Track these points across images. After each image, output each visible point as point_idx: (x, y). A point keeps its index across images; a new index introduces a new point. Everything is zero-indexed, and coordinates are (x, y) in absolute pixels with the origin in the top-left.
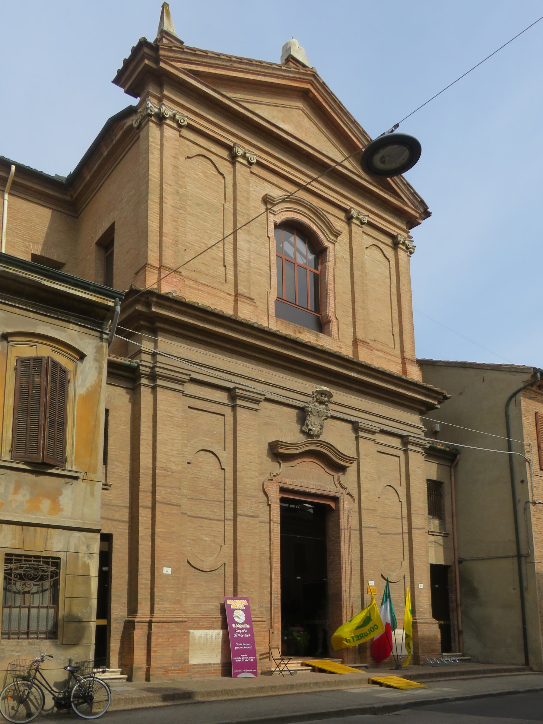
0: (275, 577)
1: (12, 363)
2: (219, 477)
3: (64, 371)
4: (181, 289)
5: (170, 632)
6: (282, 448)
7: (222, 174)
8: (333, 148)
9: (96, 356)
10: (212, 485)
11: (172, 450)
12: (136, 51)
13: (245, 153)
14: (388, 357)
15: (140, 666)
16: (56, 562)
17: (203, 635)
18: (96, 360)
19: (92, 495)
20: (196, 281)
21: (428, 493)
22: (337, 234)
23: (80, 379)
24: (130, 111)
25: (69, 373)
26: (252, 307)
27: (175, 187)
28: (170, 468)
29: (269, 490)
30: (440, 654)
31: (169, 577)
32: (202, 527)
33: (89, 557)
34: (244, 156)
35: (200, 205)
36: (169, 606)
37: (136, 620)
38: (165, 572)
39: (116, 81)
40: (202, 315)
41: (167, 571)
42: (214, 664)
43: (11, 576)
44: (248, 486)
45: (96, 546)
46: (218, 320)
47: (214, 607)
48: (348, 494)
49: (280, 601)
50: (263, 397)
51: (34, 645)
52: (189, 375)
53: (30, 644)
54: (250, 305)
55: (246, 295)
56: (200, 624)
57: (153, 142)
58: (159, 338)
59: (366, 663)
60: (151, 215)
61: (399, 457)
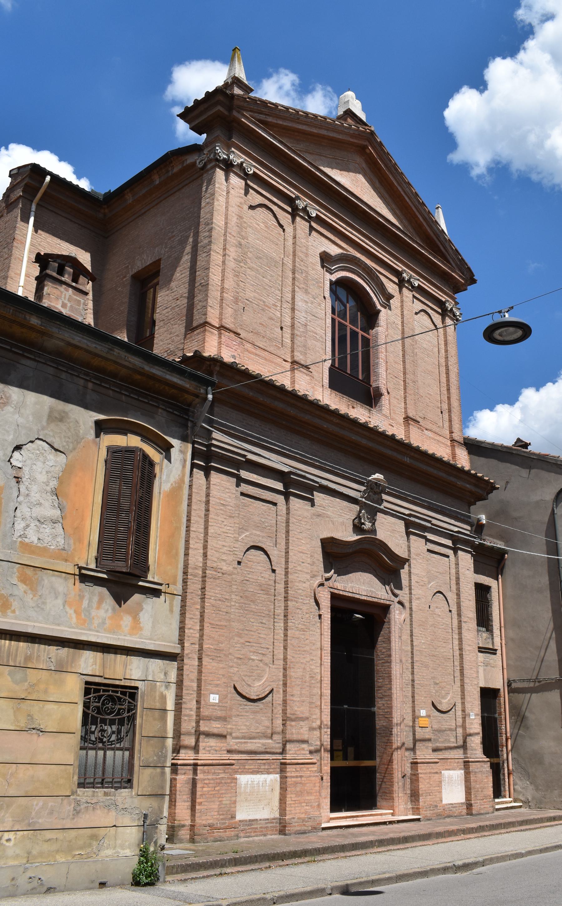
0: (325, 707)
1: (103, 454)
3: (151, 464)
4: (240, 354)
5: (217, 779)
7: (281, 226)
9: (181, 447)
10: (262, 590)
14: (438, 438)
15: (182, 823)
16: (131, 692)
17: (250, 782)
18: (181, 451)
19: (171, 611)
21: (476, 600)
23: (165, 474)
24: (194, 149)
26: (308, 378)
27: (239, 239)
28: (221, 569)
29: (320, 596)
30: (492, 801)
31: (216, 707)
33: (167, 687)
34: (305, 210)
35: (260, 258)
36: (215, 745)
38: (211, 701)
41: (214, 698)
42: (260, 820)
43: (89, 709)
51: (110, 796)
52: (244, 456)
53: (106, 794)
54: (307, 375)
55: (302, 362)
56: (246, 767)
57: (219, 188)
59: (419, 814)
60: (213, 267)
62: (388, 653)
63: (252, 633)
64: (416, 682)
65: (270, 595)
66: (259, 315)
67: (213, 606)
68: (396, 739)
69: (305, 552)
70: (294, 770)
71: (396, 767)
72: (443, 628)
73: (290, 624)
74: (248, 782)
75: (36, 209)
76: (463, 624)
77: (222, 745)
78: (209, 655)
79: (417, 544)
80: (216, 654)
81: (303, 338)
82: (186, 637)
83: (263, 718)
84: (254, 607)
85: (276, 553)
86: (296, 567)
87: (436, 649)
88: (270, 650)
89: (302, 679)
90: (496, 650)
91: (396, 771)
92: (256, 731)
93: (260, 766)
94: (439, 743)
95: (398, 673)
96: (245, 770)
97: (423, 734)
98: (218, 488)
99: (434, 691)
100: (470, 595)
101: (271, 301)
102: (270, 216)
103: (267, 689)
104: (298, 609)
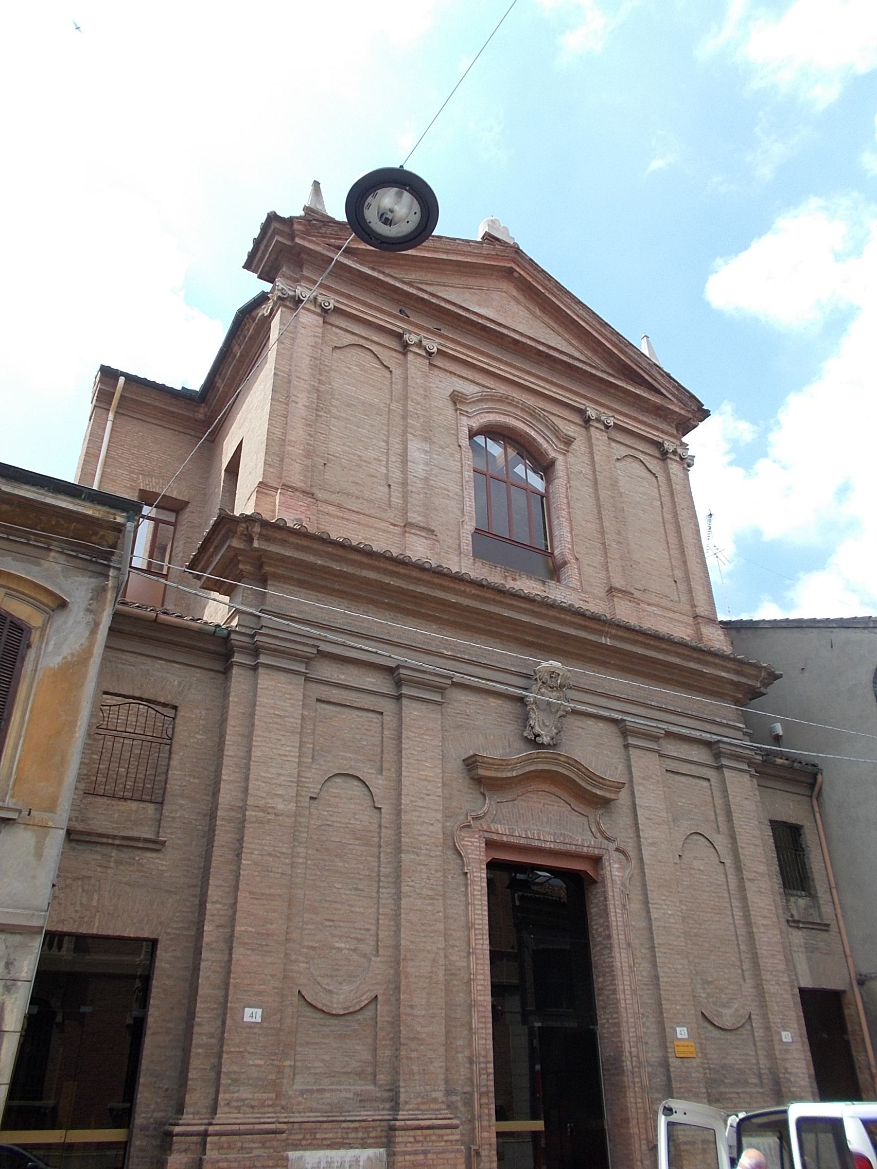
2: (370, 823)
6: (486, 769)
8: (554, 335)
10: (357, 839)
11: (279, 774)
12: (265, 228)
13: (421, 341)
14: (671, 615)
19: (39, 854)
20: (339, 506)
22: (568, 441)
23: (52, 642)
24: (262, 298)
25: (33, 631)
28: (274, 808)
31: (256, 1030)
32: (332, 921)
34: (419, 345)
36: (250, 1096)
37: (177, 1129)
39: (248, 266)
40: (631, 636)
41: (252, 1015)
44: (423, 838)
45: (26, 962)
46: (365, 560)
47: (350, 1095)
48: (617, 850)
49: (492, 1077)
50: (449, 682)
56: (318, 1136)
58: (270, 591)
61: (709, 780)
62: (607, 932)
63: (339, 906)
64: (661, 979)
65: (371, 845)
66: (352, 472)
67: (256, 864)
68: (630, 1079)
69: (432, 779)
70: (412, 1139)
71: (636, 1131)
72: (711, 891)
73: (405, 889)
74: (319, 1163)
75: (115, 418)
76: (748, 884)
77: (265, 1096)
78: (246, 944)
79: (645, 764)
80: (259, 942)
81: (422, 495)
82: (207, 917)
83: (358, 1048)
84: (341, 864)
85: (379, 784)
86: (415, 802)
87: (700, 924)
88: (372, 932)
89: (431, 977)
90: (828, 925)
91: (636, 1137)
92: (345, 1070)
93: (347, 1133)
94: (726, 1087)
95: (625, 965)
96: (314, 1142)
97: (685, 1070)
98: (272, 693)
99: (703, 995)
100: (754, 837)
101: (371, 454)
102: (369, 357)
103: (364, 997)
104: (419, 864)
